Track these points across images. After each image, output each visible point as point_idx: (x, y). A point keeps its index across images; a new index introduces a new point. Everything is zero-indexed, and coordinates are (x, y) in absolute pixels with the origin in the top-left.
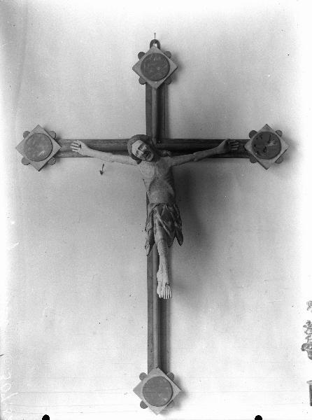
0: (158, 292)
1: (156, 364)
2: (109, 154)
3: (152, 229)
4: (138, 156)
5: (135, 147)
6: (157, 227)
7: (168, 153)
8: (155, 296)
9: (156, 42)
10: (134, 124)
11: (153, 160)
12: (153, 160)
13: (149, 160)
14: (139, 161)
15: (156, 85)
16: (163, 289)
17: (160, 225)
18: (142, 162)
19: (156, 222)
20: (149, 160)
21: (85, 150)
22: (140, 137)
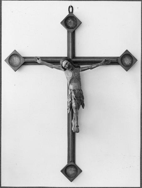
0: (73, 129)
1: (26, 60)
2: (52, 64)
3: (71, 101)
4: (65, 68)
5: (64, 63)
6: (73, 101)
7: (69, 113)
8: (70, 131)
9: (72, 7)
10: (62, 51)
11: (71, 70)
12: (71, 70)
13: (70, 69)
14: (65, 70)
15: (72, 30)
16: (75, 128)
17: (74, 99)
18: (67, 70)
19: (73, 98)
20: (70, 69)
21: (39, 61)
22: (66, 59)
